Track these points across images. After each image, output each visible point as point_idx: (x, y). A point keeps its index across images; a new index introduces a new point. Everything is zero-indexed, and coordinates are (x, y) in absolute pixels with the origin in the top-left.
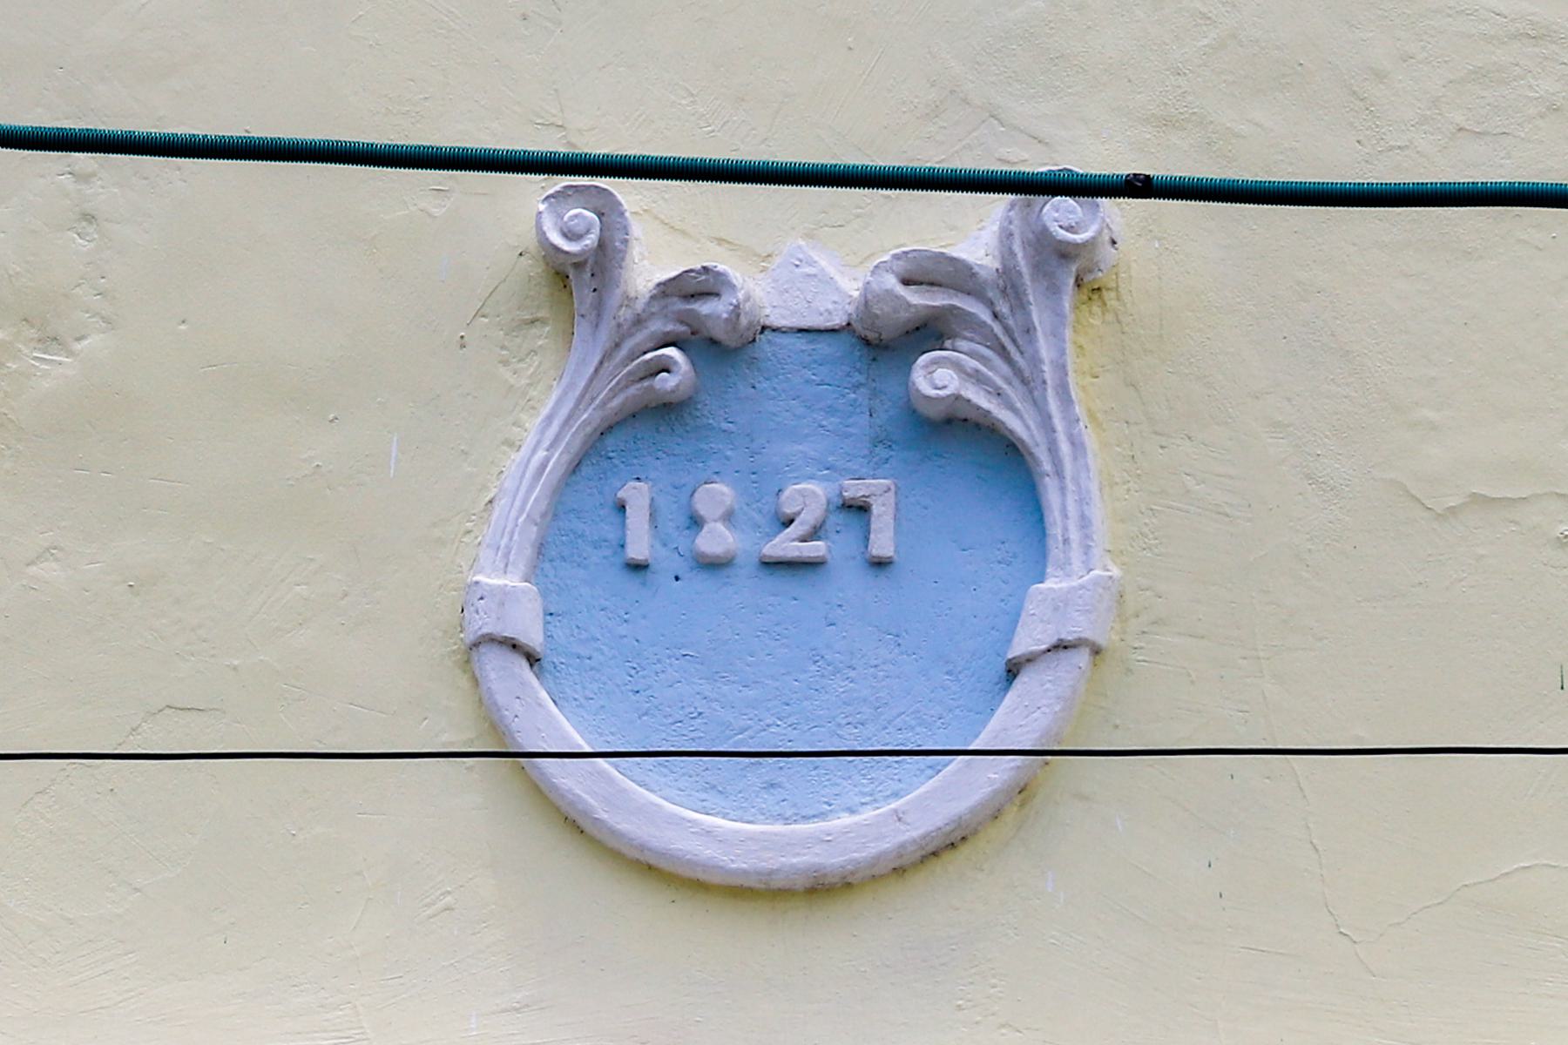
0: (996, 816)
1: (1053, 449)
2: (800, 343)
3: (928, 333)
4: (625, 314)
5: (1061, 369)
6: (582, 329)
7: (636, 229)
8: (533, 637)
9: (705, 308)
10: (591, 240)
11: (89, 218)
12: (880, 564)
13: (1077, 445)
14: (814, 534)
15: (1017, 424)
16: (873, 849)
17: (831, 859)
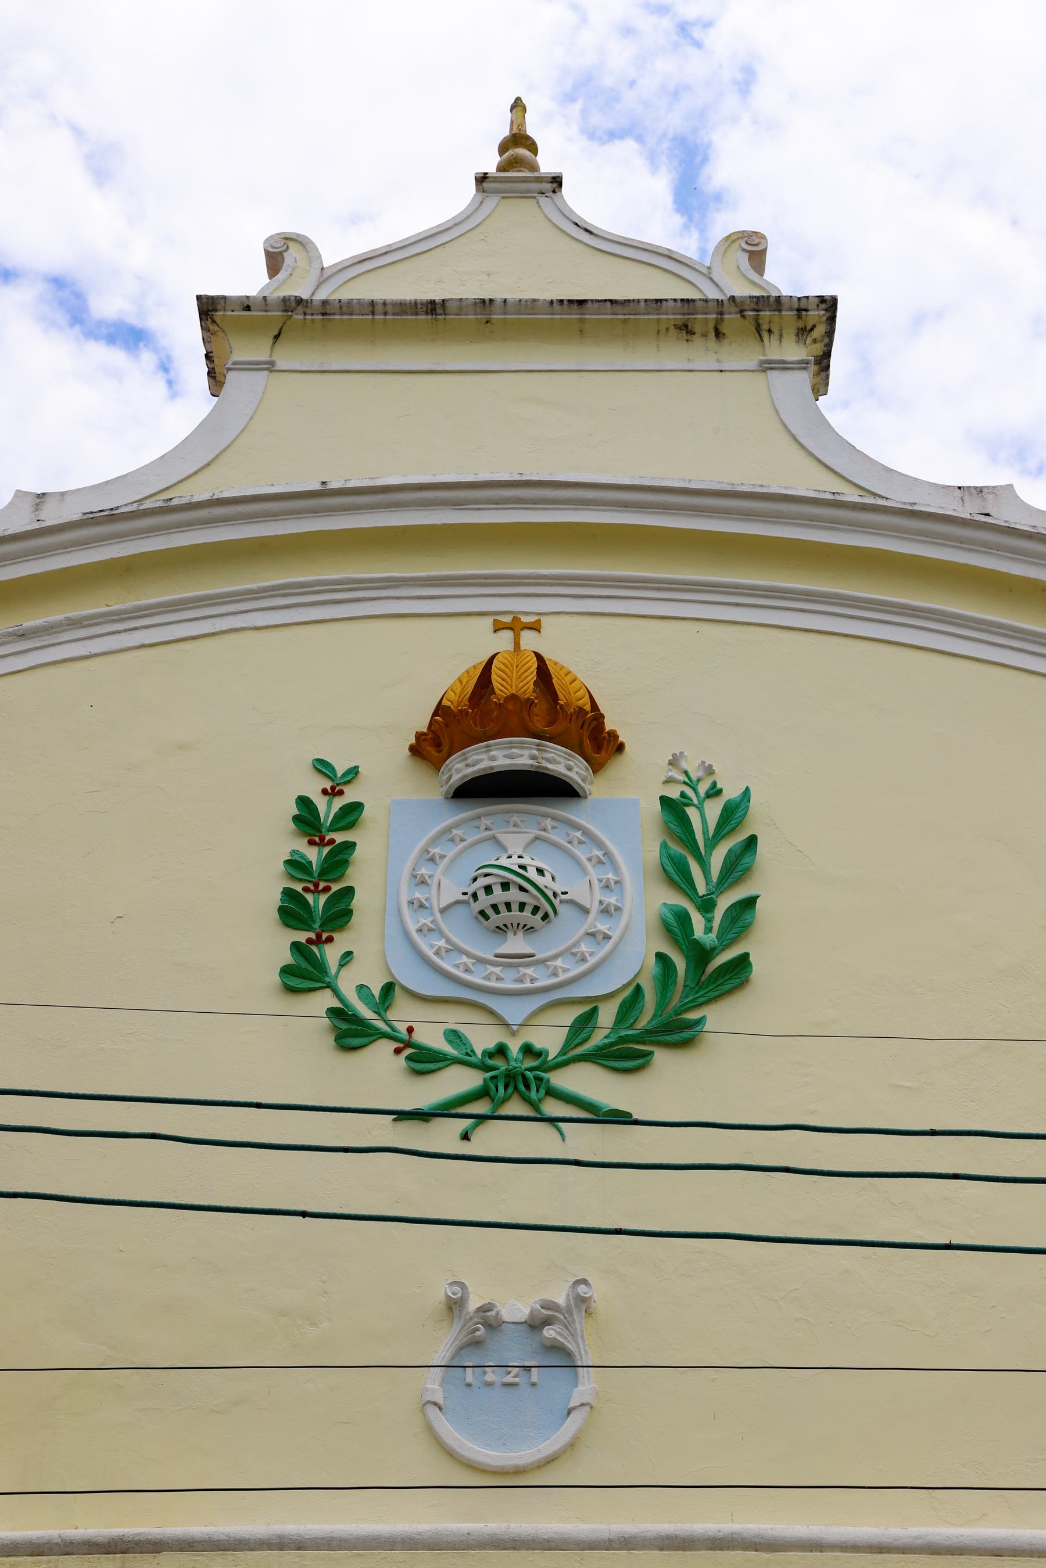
0: (565, 1452)
1: (580, 1354)
2: (513, 1326)
3: (547, 1322)
4: (468, 1317)
5: (582, 1331)
6: (456, 1321)
7: (471, 1297)
8: (441, 1402)
9: (489, 1314)
10: (459, 1295)
11: (325, 1292)
12: (534, 1384)
13: (585, 1351)
14: (516, 1376)
15: (571, 1346)
16: (532, 1460)
17: (521, 1462)
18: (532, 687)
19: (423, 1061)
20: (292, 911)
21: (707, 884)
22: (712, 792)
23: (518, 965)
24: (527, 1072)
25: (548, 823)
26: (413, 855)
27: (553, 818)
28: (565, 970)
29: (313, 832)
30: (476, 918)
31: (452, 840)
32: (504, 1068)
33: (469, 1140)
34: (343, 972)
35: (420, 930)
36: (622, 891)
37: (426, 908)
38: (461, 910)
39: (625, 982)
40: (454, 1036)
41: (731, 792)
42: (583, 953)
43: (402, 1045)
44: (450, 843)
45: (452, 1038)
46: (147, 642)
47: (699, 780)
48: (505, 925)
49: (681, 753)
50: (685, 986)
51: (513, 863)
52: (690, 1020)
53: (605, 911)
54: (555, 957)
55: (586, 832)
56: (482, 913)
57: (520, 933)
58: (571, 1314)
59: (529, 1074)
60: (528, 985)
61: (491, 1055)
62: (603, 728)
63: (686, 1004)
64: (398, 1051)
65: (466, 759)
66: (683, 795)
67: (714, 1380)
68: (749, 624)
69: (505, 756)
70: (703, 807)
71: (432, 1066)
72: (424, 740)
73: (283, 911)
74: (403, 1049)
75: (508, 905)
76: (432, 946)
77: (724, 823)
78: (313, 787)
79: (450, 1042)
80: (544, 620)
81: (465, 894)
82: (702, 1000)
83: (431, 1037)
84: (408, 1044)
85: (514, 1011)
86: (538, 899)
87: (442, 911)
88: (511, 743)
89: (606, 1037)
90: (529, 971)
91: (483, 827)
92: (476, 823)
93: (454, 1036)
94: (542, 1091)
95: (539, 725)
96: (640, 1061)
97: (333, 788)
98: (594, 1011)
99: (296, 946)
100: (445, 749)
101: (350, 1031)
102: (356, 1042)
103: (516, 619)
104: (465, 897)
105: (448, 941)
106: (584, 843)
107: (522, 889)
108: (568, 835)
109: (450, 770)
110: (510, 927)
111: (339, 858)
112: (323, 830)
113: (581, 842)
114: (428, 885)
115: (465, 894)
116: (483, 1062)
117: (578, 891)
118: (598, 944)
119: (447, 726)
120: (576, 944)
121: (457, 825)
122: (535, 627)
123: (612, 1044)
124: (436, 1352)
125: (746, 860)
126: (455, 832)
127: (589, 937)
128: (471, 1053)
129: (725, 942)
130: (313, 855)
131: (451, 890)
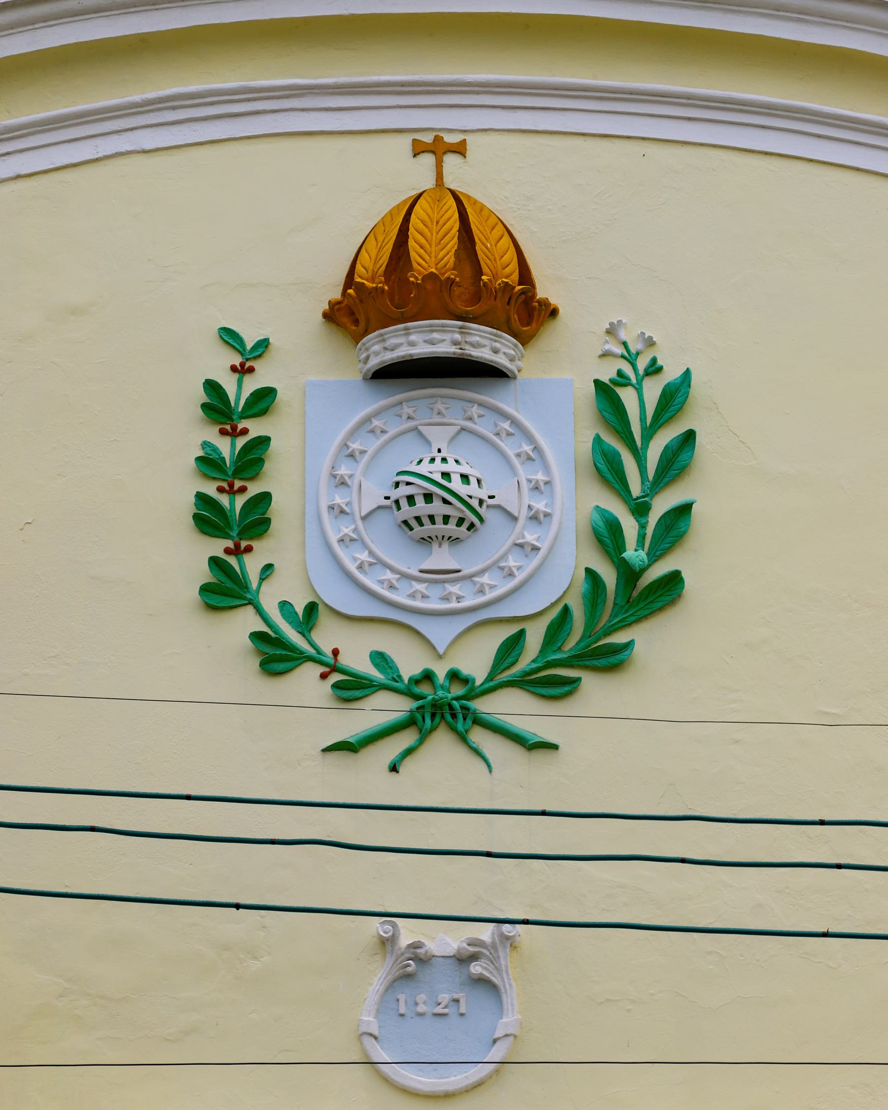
0: (491, 1077)
1: (505, 986)
2: (442, 960)
3: (474, 957)
4: (399, 952)
5: (507, 967)
6: (388, 955)
8: (376, 1032)
9: (419, 951)
10: (390, 934)
11: (264, 927)
12: (462, 1015)
13: (511, 986)
14: (446, 1007)
17: (450, 1088)
18: (453, 259)
19: (352, 689)
20: (208, 518)
21: (643, 483)
22: (651, 370)
23: (444, 581)
24: (455, 703)
25: (475, 410)
26: (331, 443)
27: (481, 405)
28: (492, 587)
29: (224, 420)
30: (400, 526)
31: (372, 431)
32: (430, 698)
33: (398, 772)
34: (265, 587)
35: (341, 540)
36: (552, 495)
37: (347, 514)
38: (383, 516)
39: (553, 600)
40: (380, 659)
41: (671, 373)
42: (510, 568)
43: (327, 670)
44: (370, 435)
45: (378, 661)
46: (23, 172)
47: (638, 354)
48: (430, 537)
49: (619, 322)
50: (615, 604)
51: (435, 470)
52: (617, 645)
53: (534, 518)
54: (482, 572)
55: (514, 422)
56: (405, 522)
57: (446, 545)
58: (496, 950)
59: (456, 704)
60: (454, 605)
61: (417, 681)
62: (534, 295)
63: (612, 625)
64: (324, 676)
65: (384, 340)
66: (620, 374)
67: (629, 1011)
68: (702, 145)
69: (425, 341)
70: (641, 388)
71: (358, 693)
72: (339, 309)
73: (198, 519)
74: (330, 673)
75: (432, 518)
76: (355, 559)
77: (662, 410)
78: (219, 365)
79: (376, 665)
80: (470, 139)
81: (387, 498)
82: (633, 618)
83: (356, 660)
84: (334, 669)
85: (440, 634)
86: (463, 511)
87: (364, 518)
88: (431, 326)
89: (533, 661)
90: (455, 589)
91: (405, 417)
92: (397, 409)
93: (380, 659)
94: (469, 721)
95: (461, 307)
96: (567, 688)
97: (242, 365)
98: (521, 633)
99: (214, 561)
100: (362, 325)
101: (275, 655)
102: (281, 666)
103: (438, 139)
104: (388, 502)
105: (371, 553)
106: (512, 434)
107: (445, 501)
108: (496, 425)
109: (367, 349)
110: (435, 538)
111: (254, 456)
112: (235, 417)
113: (509, 434)
114: (348, 486)
115: (387, 498)
116: (409, 690)
117: (507, 497)
118: (527, 556)
119: (361, 301)
120: (504, 557)
121: (376, 414)
122: (460, 149)
123: (539, 669)
124: (371, 985)
125: (683, 456)
126: (376, 423)
127: (517, 549)
128: (398, 678)
129: (658, 553)
130: (226, 448)
131: (374, 492)
